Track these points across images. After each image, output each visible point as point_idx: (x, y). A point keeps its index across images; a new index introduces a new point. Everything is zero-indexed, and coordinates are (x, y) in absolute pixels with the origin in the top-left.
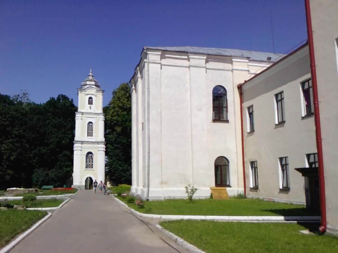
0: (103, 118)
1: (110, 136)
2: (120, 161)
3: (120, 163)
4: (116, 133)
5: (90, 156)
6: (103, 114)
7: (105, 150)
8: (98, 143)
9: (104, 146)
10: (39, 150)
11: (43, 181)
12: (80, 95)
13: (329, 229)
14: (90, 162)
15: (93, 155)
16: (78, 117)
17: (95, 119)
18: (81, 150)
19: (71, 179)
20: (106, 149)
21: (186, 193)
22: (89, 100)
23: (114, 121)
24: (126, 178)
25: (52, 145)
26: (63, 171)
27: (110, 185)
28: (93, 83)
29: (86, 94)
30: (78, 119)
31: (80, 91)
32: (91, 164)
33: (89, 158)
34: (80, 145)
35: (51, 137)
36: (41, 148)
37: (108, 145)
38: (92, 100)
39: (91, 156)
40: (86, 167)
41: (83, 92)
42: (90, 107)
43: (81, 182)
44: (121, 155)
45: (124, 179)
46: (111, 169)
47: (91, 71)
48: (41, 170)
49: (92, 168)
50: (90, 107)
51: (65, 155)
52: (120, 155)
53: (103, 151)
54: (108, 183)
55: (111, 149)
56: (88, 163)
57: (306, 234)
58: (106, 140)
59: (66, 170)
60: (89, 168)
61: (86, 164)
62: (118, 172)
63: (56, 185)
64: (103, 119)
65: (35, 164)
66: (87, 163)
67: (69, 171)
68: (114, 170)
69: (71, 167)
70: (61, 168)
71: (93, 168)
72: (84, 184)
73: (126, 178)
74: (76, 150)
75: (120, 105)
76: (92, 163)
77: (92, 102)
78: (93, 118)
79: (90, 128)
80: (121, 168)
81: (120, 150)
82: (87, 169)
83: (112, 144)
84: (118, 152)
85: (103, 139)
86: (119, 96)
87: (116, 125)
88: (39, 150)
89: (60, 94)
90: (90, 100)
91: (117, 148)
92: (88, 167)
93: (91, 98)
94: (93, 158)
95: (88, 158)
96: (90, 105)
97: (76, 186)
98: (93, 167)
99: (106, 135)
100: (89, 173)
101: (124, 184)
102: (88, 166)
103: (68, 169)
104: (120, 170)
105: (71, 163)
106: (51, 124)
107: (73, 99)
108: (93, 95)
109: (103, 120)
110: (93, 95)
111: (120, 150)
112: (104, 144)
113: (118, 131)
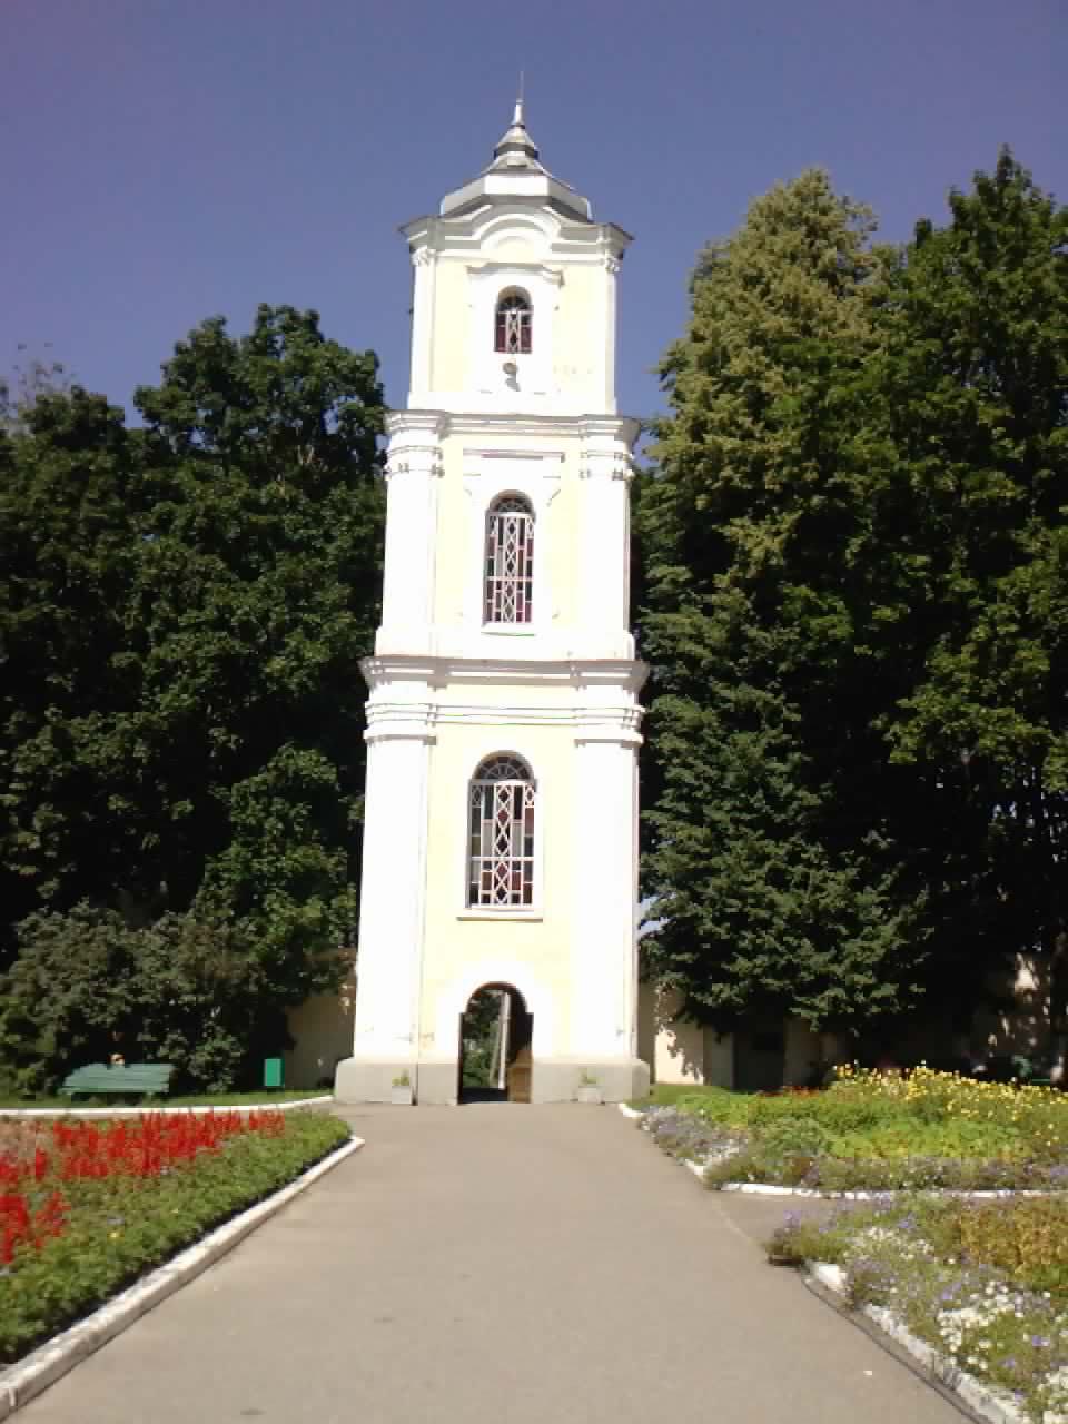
0: (619, 456)
1: (682, 621)
2: (778, 833)
3: (777, 850)
4: (735, 582)
5: (504, 797)
6: (619, 423)
7: (639, 739)
8: (576, 671)
9: (628, 701)
10: (64, 743)
11: (75, 1018)
12: (424, 275)
14: (502, 845)
15: (534, 788)
16: (405, 449)
17: (552, 464)
18: (431, 741)
19: (187, 1009)
20: (646, 726)
22: (500, 320)
23: (715, 470)
24: (840, 992)
25: (175, 688)
26: (261, 931)
27: (680, 1057)
28: (538, 185)
29: (480, 265)
30: (405, 469)
31: (429, 241)
32: (516, 865)
33: (505, 546)
35: (171, 626)
36: (78, 726)
37: (663, 703)
38: (526, 320)
39: (518, 791)
40: (473, 897)
41: (448, 252)
42: (511, 369)
44: (790, 777)
45: (821, 1002)
46: (693, 909)
47: (518, 117)
48: (79, 918)
49: (522, 906)
50: (511, 369)
51: (294, 787)
52: (774, 781)
53: (625, 744)
54: (664, 1040)
55: (693, 735)
56: (493, 859)
57: (30, 875)
58: (642, 654)
59: (292, 920)
60: (500, 906)
61: (471, 866)
62: (769, 939)
63: (201, 1057)
64: (621, 466)
65: (29, 870)
66: (482, 858)
68: (717, 921)
69: (338, 890)
70: (247, 900)
71: (528, 900)
72: (446, 1048)
73: (840, 992)
74: (389, 738)
75: (774, 322)
76: (523, 859)
77: (527, 332)
79: (511, 547)
80: (786, 902)
81: (771, 735)
82: (478, 910)
83: (694, 689)
84: (757, 751)
85: (623, 645)
86: (754, 266)
87: (732, 503)
88: (64, 743)
89: (274, 306)
90: (508, 319)
91: (746, 718)
92: (493, 893)
93: (514, 300)
94: (530, 813)
95: (501, 543)
96: (506, 357)
97: (376, 1070)
98: (528, 890)
101: (906, 1064)
102: (487, 877)
103: (312, 910)
104: (780, 923)
105: (342, 853)
106: (179, 522)
107: (377, 351)
108: (535, 268)
109: (617, 476)
110: (535, 268)
111: (771, 735)
112: (626, 685)
113: (758, 553)
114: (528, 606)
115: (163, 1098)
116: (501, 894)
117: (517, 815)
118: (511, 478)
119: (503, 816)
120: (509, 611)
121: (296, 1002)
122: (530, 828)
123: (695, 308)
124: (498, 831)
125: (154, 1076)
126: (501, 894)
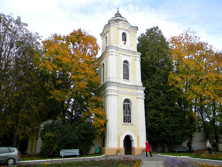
7: (144, 98)
13: (138, 57)
14: (127, 113)
17: (131, 58)
21: (201, 140)
30: (112, 54)
32: (129, 116)
34: (115, 88)
38: (125, 37)
43: (119, 144)
67: (104, 131)
72: (122, 145)
76: (129, 115)
78: (130, 56)
85: (141, 84)
98: (130, 120)
99: (143, 79)
100: (128, 130)
114: (128, 77)
115: (80, 156)
116: (127, 121)
117: (128, 109)
118: (126, 58)
119: (126, 109)
120: (126, 78)
121: (93, 139)
122: (130, 111)
123: (175, 37)
124: (126, 111)
125: (76, 152)
126: (127, 121)
